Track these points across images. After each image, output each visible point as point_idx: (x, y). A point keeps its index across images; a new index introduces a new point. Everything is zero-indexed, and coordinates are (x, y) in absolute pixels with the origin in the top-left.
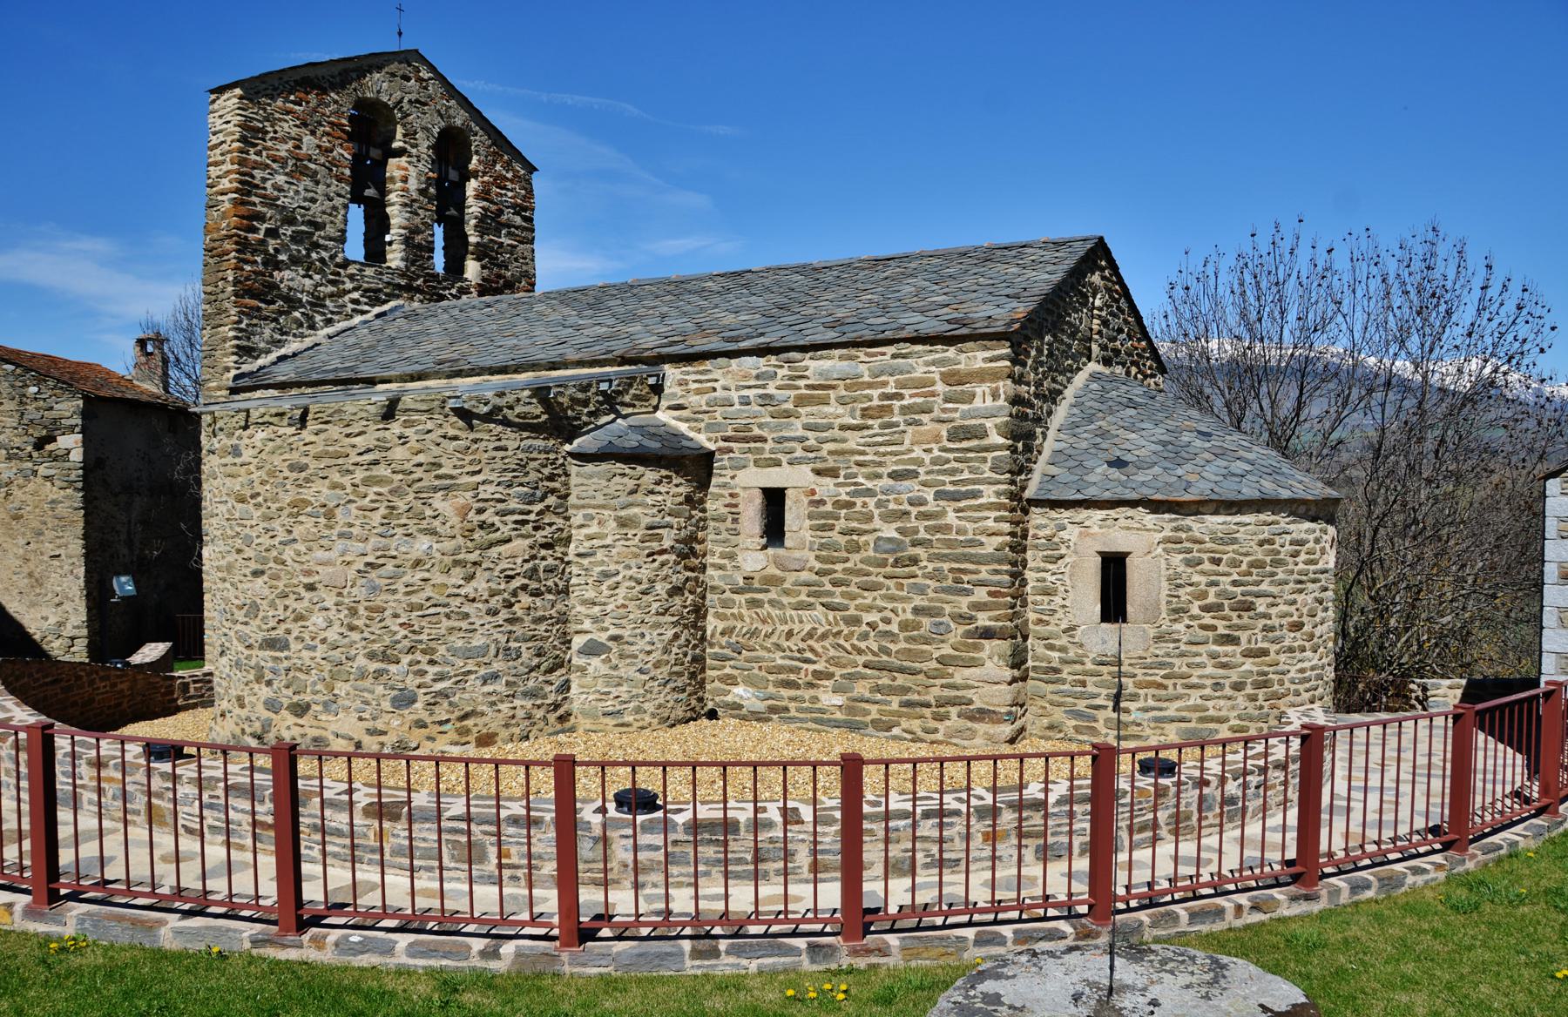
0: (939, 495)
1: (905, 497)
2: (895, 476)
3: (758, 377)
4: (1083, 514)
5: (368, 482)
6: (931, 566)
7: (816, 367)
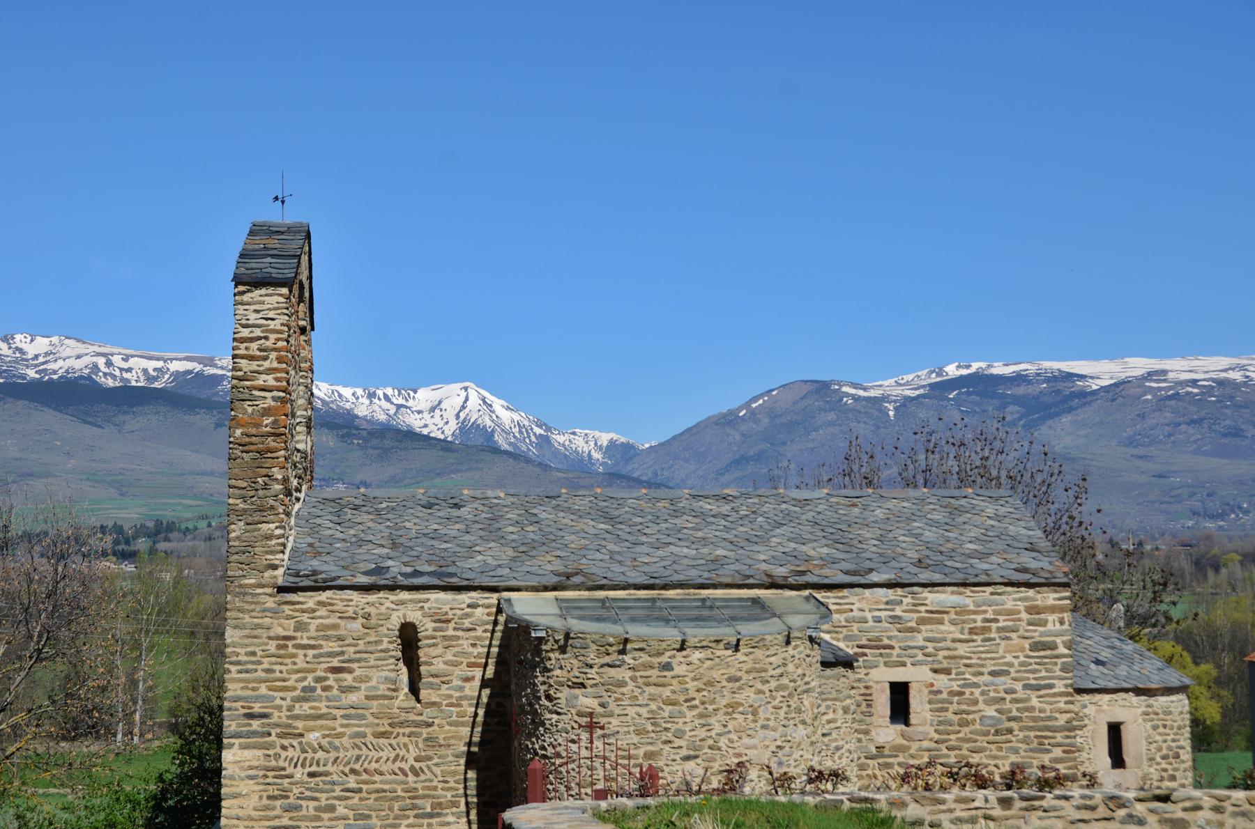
0: (1026, 687)
1: (1001, 688)
2: (992, 674)
3: (887, 603)
4: (1097, 697)
5: (778, 688)
6: (1021, 735)
7: (934, 598)
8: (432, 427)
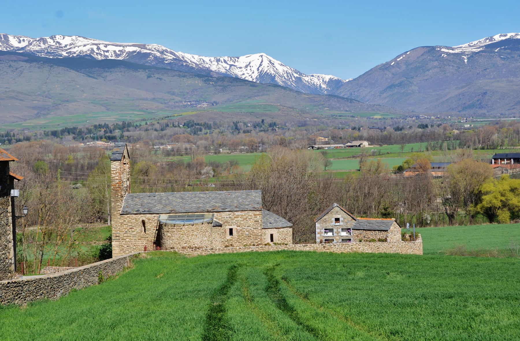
7: (237, 213)
8: (246, 75)
